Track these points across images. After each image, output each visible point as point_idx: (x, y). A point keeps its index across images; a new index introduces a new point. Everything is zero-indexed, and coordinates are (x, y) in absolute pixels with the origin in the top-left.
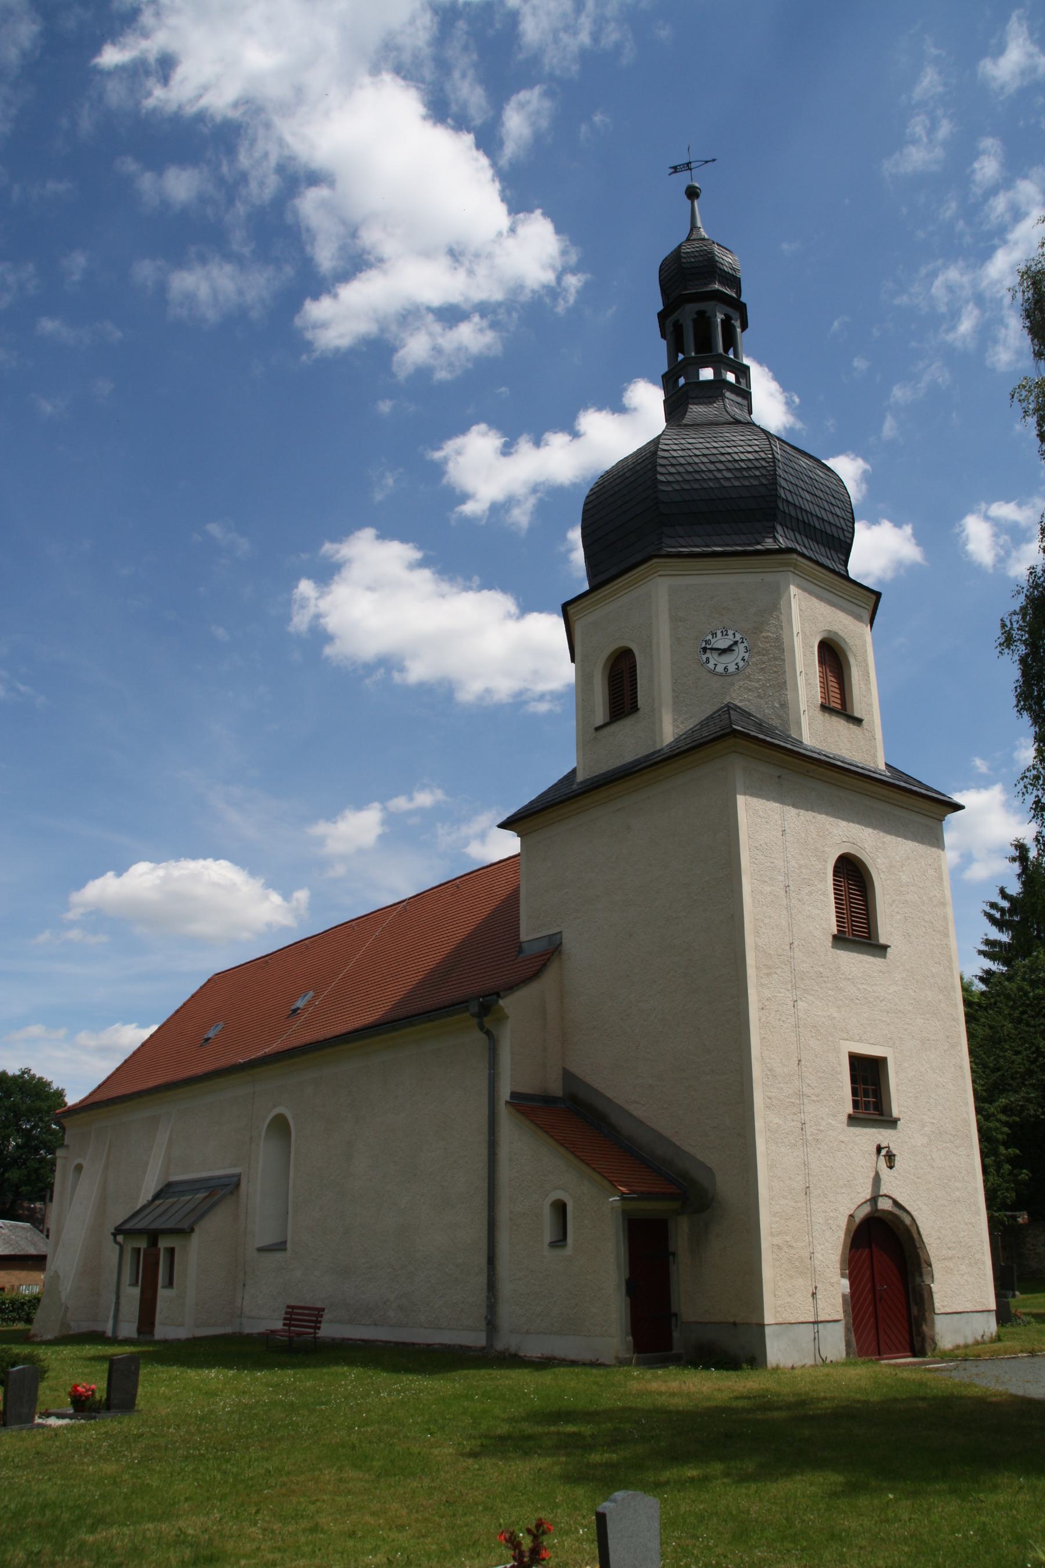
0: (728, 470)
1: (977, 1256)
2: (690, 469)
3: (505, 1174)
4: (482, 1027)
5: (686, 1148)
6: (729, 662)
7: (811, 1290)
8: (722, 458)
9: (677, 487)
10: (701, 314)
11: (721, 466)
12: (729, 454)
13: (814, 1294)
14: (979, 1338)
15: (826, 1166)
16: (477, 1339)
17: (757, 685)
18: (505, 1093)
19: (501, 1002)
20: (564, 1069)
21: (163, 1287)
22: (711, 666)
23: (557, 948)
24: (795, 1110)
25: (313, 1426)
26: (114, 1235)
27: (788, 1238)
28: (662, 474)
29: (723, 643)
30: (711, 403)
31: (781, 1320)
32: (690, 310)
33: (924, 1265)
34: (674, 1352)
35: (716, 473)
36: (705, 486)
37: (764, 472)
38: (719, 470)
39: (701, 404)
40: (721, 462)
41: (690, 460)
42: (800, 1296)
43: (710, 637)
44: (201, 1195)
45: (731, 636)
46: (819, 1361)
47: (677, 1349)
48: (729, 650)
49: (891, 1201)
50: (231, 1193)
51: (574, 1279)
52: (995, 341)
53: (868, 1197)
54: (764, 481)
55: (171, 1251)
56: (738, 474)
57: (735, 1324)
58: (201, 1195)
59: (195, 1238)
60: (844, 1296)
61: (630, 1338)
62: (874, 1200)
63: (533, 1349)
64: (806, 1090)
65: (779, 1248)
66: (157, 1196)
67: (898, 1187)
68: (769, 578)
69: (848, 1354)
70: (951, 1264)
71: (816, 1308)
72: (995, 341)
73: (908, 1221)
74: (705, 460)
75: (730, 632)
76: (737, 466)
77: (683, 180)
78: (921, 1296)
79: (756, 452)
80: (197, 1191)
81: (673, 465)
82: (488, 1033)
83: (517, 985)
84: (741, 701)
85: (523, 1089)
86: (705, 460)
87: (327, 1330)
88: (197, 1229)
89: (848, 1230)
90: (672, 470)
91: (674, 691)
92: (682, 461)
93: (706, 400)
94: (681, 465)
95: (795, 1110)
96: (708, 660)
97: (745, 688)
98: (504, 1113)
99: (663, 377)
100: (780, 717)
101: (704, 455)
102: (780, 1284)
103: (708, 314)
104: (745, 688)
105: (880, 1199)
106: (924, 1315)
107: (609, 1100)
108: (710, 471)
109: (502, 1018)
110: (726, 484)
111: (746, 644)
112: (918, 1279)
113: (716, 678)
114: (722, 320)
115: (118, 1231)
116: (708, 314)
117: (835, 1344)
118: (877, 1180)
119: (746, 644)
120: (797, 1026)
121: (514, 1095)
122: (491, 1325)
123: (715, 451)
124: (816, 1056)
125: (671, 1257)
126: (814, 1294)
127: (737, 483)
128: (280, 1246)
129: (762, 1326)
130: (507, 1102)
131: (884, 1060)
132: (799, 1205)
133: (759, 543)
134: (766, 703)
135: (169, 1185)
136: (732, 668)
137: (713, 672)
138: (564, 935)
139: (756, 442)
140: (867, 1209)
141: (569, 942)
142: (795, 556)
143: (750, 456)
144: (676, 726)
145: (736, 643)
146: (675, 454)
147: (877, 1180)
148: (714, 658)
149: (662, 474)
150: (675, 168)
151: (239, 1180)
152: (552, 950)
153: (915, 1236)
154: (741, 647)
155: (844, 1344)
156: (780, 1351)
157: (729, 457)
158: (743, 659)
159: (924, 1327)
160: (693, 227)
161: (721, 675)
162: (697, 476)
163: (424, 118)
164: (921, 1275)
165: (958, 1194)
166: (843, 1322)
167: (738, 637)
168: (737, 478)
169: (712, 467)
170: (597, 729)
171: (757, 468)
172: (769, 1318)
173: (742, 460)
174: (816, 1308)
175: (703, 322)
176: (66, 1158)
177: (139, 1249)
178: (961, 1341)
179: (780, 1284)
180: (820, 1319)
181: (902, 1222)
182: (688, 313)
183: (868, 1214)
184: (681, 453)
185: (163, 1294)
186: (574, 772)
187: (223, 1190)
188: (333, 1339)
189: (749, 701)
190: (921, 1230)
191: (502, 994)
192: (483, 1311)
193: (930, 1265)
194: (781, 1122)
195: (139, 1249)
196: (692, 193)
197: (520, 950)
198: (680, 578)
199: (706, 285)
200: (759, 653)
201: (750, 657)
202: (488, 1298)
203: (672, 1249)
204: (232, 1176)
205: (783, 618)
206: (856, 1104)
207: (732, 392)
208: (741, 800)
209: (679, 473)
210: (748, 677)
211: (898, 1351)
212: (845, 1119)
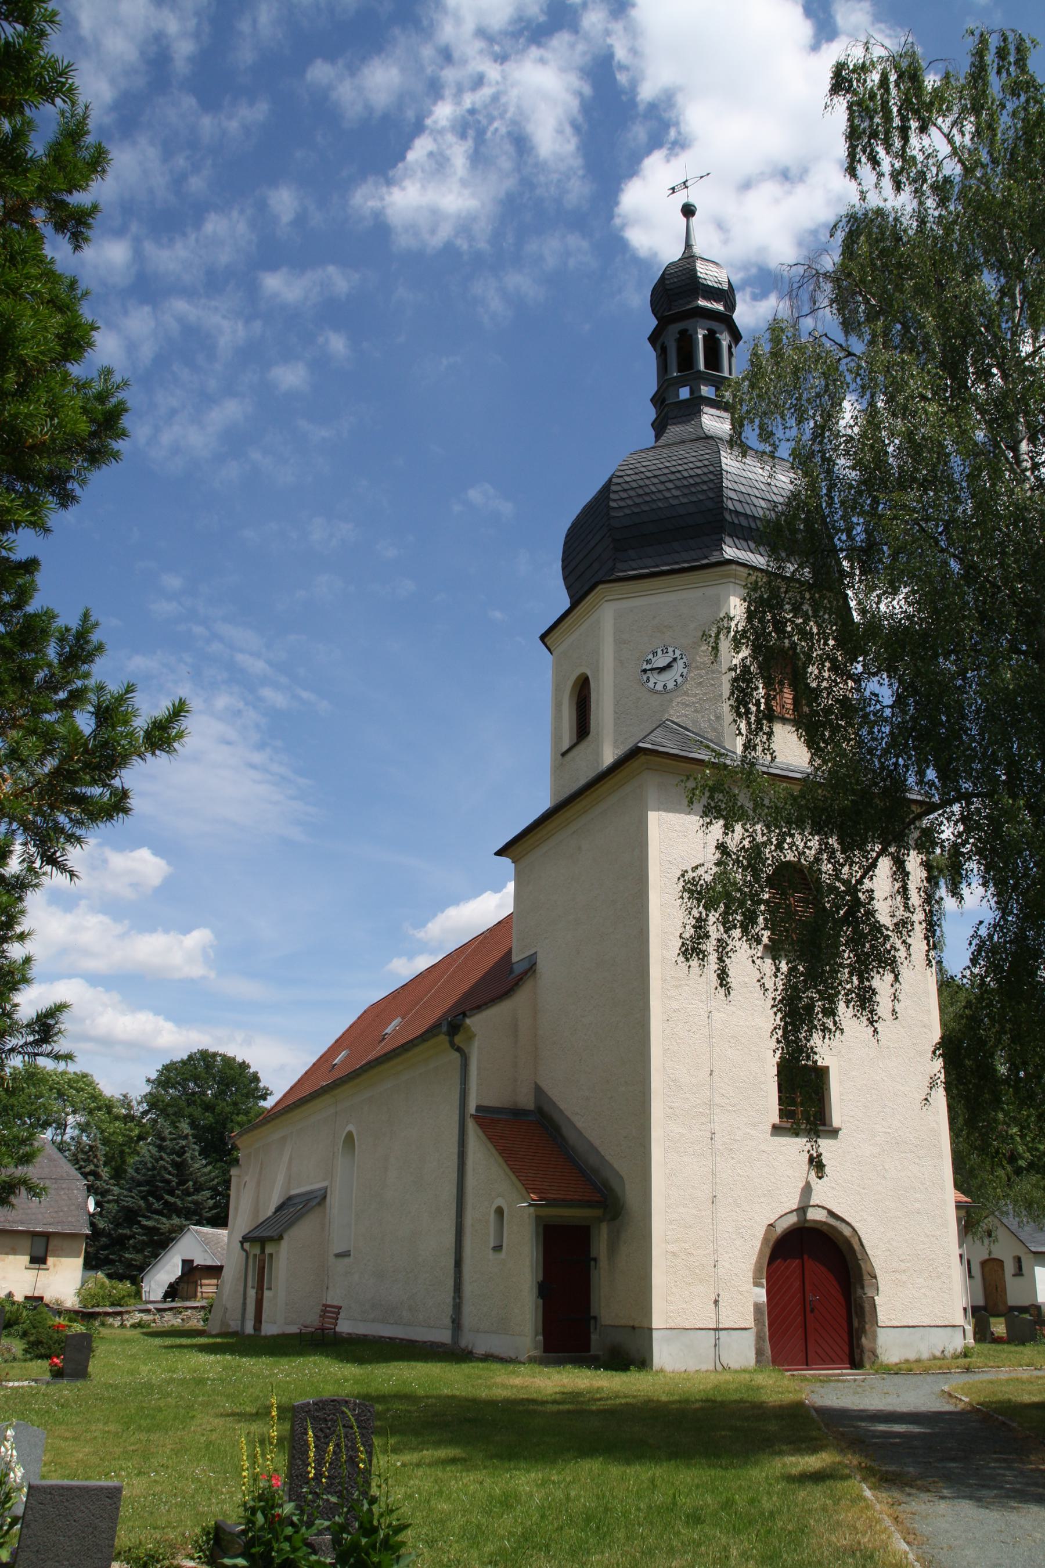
0: (677, 488)
1: (941, 1269)
2: (640, 492)
3: (471, 1181)
5: (608, 1158)
6: (668, 679)
7: (713, 1297)
8: (672, 477)
9: (628, 511)
11: (670, 485)
12: (679, 471)
13: (716, 1302)
14: (938, 1354)
15: (740, 1176)
16: (444, 1336)
17: (694, 700)
18: (472, 1109)
19: (468, 1021)
20: (536, 1084)
22: (651, 685)
23: (531, 968)
24: (703, 1119)
26: (242, 1243)
27: (686, 1246)
28: (615, 500)
29: (661, 661)
30: (689, 421)
31: (672, 1325)
33: (866, 1277)
34: (592, 1353)
35: (665, 493)
36: (654, 506)
37: (712, 485)
38: (668, 489)
39: (679, 423)
40: (671, 481)
41: (641, 483)
42: (700, 1301)
43: (651, 656)
45: (671, 654)
46: (719, 1368)
47: (595, 1350)
48: (669, 666)
49: (825, 1212)
50: (319, 1204)
51: (509, 1282)
52: (771, 340)
53: (795, 1207)
54: (711, 495)
55: (271, 1255)
56: (686, 491)
57: (633, 1328)
59: (284, 1244)
60: (757, 1307)
61: (540, 1338)
62: (802, 1210)
63: (480, 1350)
64: (717, 1100)
65: (674, 1254)
66: (279, 1208)
67: (837, 1198)
68: (710, 591)
69: (758, 1361)
70: (904, 1278)
71: (717, 1314)
72: (771, 340)
73: (847, 1232)
74: (655, 481)
75: (670, 650)
76: (686, 483)
77: (681, 198)
78: (862, 1308)
79: (705, 466)
81: (625, 490)
82: (459, 1050)
83: (486, 1004)
84: (678, 717)
85: (486, 1103)
86: (655, 481)
87: (344, 1327)
88: (285, 1237)
89: (765, 1240)
91: (616, 713)
92: (634, 485)
93: (684, 419)
94: (633, 489)
95: (703, 1119)
96: (648, 679)
97: (683, 704)
98: (471, 1126)
99: (652, 400)
100: (715, 730)
101: (655, 476)
102: (674, 1290)
103: (690, 332)
104: (683, 704)
105: (810, 1210)
106: (864, 1327)
107: (561, 1111)
108: (660, 491)
109: (471, 1037)
111: (685, 660)
112: (859, 1291)
113: (655, 696)
114: (704, 336)
116: (690, 332)
117: (742, 1352)
118: (807, 1190)
119: (685, 660)
120: (710, 1037)
121: (479, 1108)
122: (456, 1323)
123: (666, 471)
124: (734, 1066)
125: (592, 1263)
126: (716, 1302)
127: (684, 500)
129: (651, 1329)
130: (472, 1115)
132: (703, 1213)
133: (706, 558)
134: (703, 717)
135: (290, 1198)
136: (671, 685)
137: (653, 691)
138: (538, 954)
139: (707, 456)
140: (793, 1219)
141: (542, 965)
142: (734, 567)
143: (699, 471)
144: (616, 747)
145: (675, 659)
146: (628, 479)
147: (807, 1190)
148: (654, 678)
149: (615, 500)
150: (673, 189)
151: (326, 1192)
152: (531, 968)
153: (857, 1247)
154: (680, 663)
155: (754, 1352)
156: (666, 1356)
157: (678, 475)
158: (682, 676)
159: (864, 1340)
161: (660, 693)
162: (647, 499)
164: (863, 1288)
165: (917, 1205)
166: (754, 1330)
167: (678, 653)
169: (662, 487)
170: (564, 754)
171: (705, 482)
172: (657, 1322)
173: (691, 476)
174: (717, 1314)
175: (686, 341)
176: (239, 1176)
178: (912, 1356)
179: (674, 1290)
180: (721, 1326)
181: (841, 1233)
182: (673, 331)
183: (794, 1224)
184: (634, 477)
187: (317, 1200)
188: (374, 1337)
189: (686, 716)
190: (864, 1241)
191: (468, 1013)
192: (449, 1311)
193: (875, 1277)
194: (684, 1132)
196: (688, 211)
197: (511, 971)
198: (624, 601)
199: (689, 303)
200: (697, 668)
201: (689, 672)
202: (454, 1298)
203: (593, 1254)
204: (320, 1190)
206: (782, 1114)
207: (712, 407)
208: (653, 817)
209: (630, 497)
210: (686, 693)
211: (833, 1362)
212: (769, 1129)
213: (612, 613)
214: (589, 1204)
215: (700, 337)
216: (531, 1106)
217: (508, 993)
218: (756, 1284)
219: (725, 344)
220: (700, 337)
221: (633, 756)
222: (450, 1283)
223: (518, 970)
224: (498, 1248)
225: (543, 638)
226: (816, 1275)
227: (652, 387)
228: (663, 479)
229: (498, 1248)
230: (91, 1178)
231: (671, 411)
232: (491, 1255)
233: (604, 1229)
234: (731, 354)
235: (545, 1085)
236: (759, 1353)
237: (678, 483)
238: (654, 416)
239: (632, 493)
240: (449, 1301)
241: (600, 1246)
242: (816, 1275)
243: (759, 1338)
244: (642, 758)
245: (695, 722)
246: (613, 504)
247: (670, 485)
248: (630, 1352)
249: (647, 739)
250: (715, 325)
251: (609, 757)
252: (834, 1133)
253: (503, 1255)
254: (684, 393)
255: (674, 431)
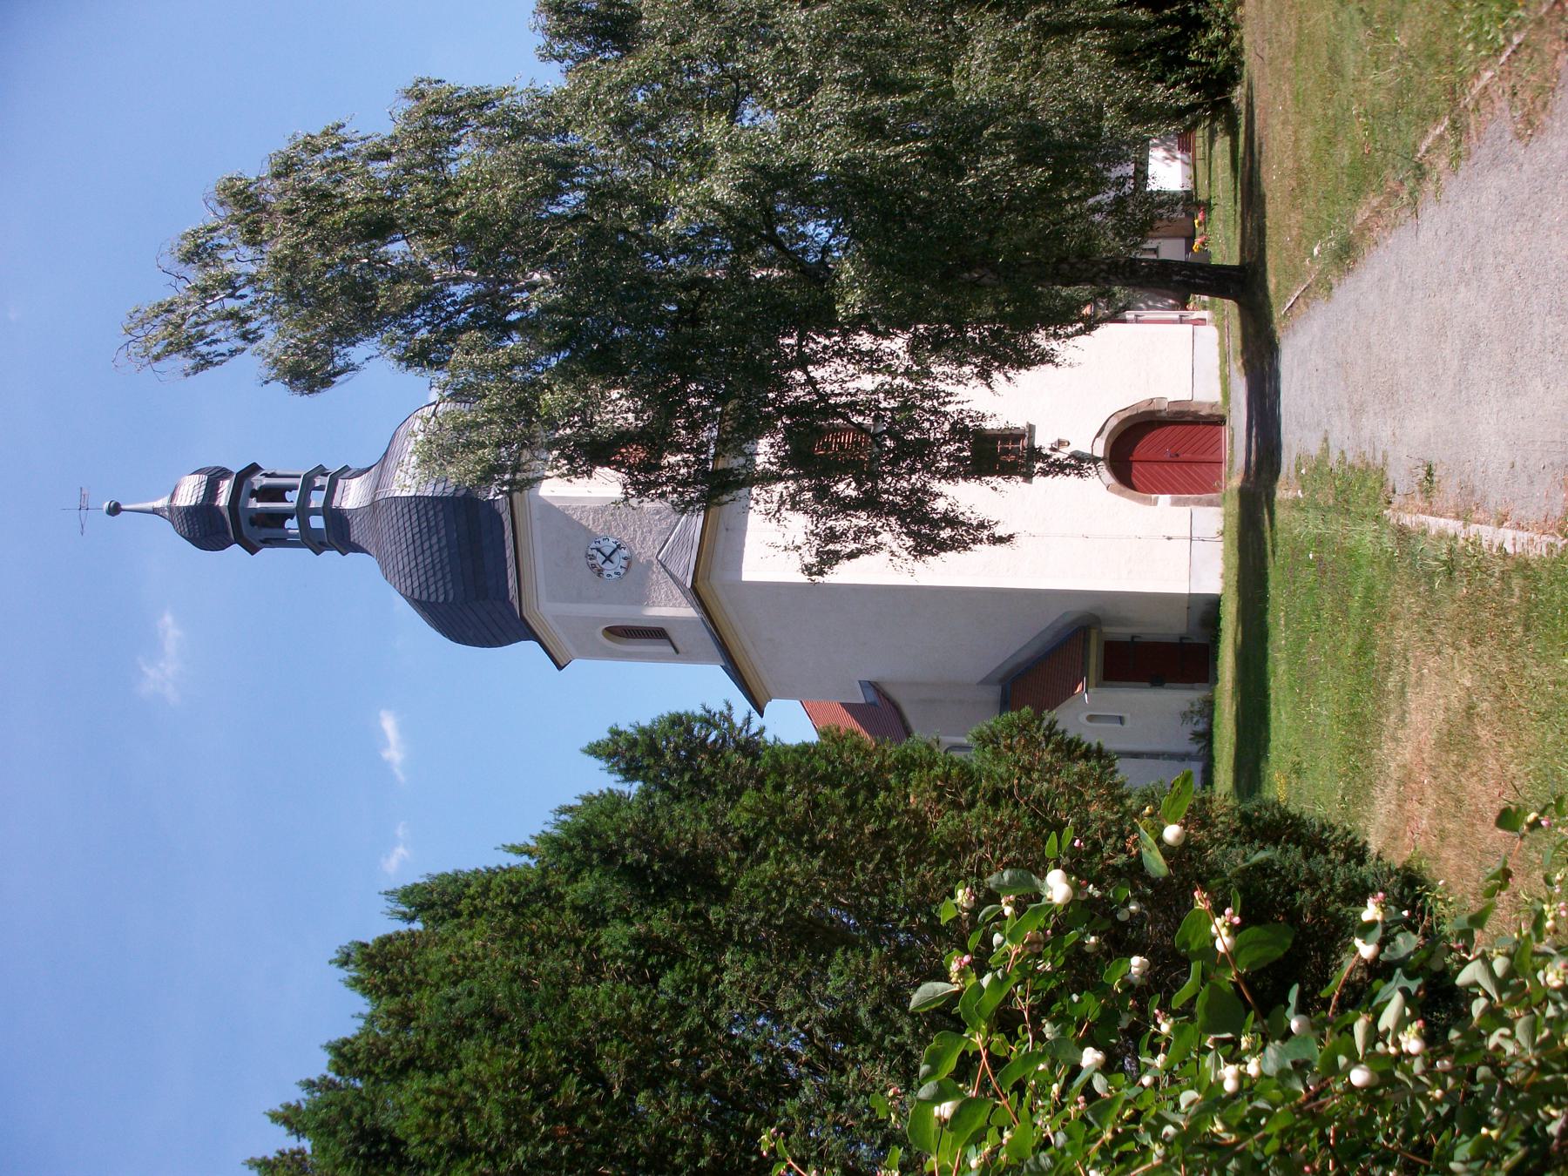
2: (431, 573)
8: (418, 543)
10: (253, 522)
11: (426, 545)
21: (1216, 421)
33: (1151, 408)
38: (431, 547)
42: (1165, 551)
60: (1175, 503)
73: (1114, 422)
78: (1177, 413)
86: (420, 559)
89: (1119, 493)
90: (432, 588)
92: (423, 578)
110: (444, 542)
122: (1183, 757)
127: (443, 532)
143: (415, 517)
146: (416, 584)
152: (874, 686)
153: (1127, 414)
160: (155, 511)
168: (438, 532)
169: (428, 553)
196: (115, 510)
197: (874, 704)
205: (575, 505)
210: (633, 540)
213: (543, 601)
214: (1086, 640)
215: (259, 505)
216: (998, 689)
217: (896, 708)
218: (1156, 503)
219: (266, 481)
220: (259, 505)
221: (697, 595)
222: (1151, 762)
223: (872, 697)
224: (1121, 720)
225: (560, 668)
226: (1146, 449)
227: (307, 553)
228: (419, 551)
229: (1121, 720)
230: (504, 360)
231: (338, 534)
232: (1127, 725)
233: (1106, 629)
234: (273, 475)
235: (980, 678)
236: (1210, 503)
237: (425, 537)
238: (336, 553)
239: (432, 580)
240: (1167, 763)
241: (1120, 632)
242: (1146, 449)
243: (1198, 503)
244: (703, 590)
245: (660, 533)
246: (441, 599)
247: (426, 545)
248: (1208, 609)
249: (682, 579)
250: (244, 491)
251: (689, 612)
252: (1031, 428)
253: (1127, 716)
254: (317, 522)
255: (356, 535)
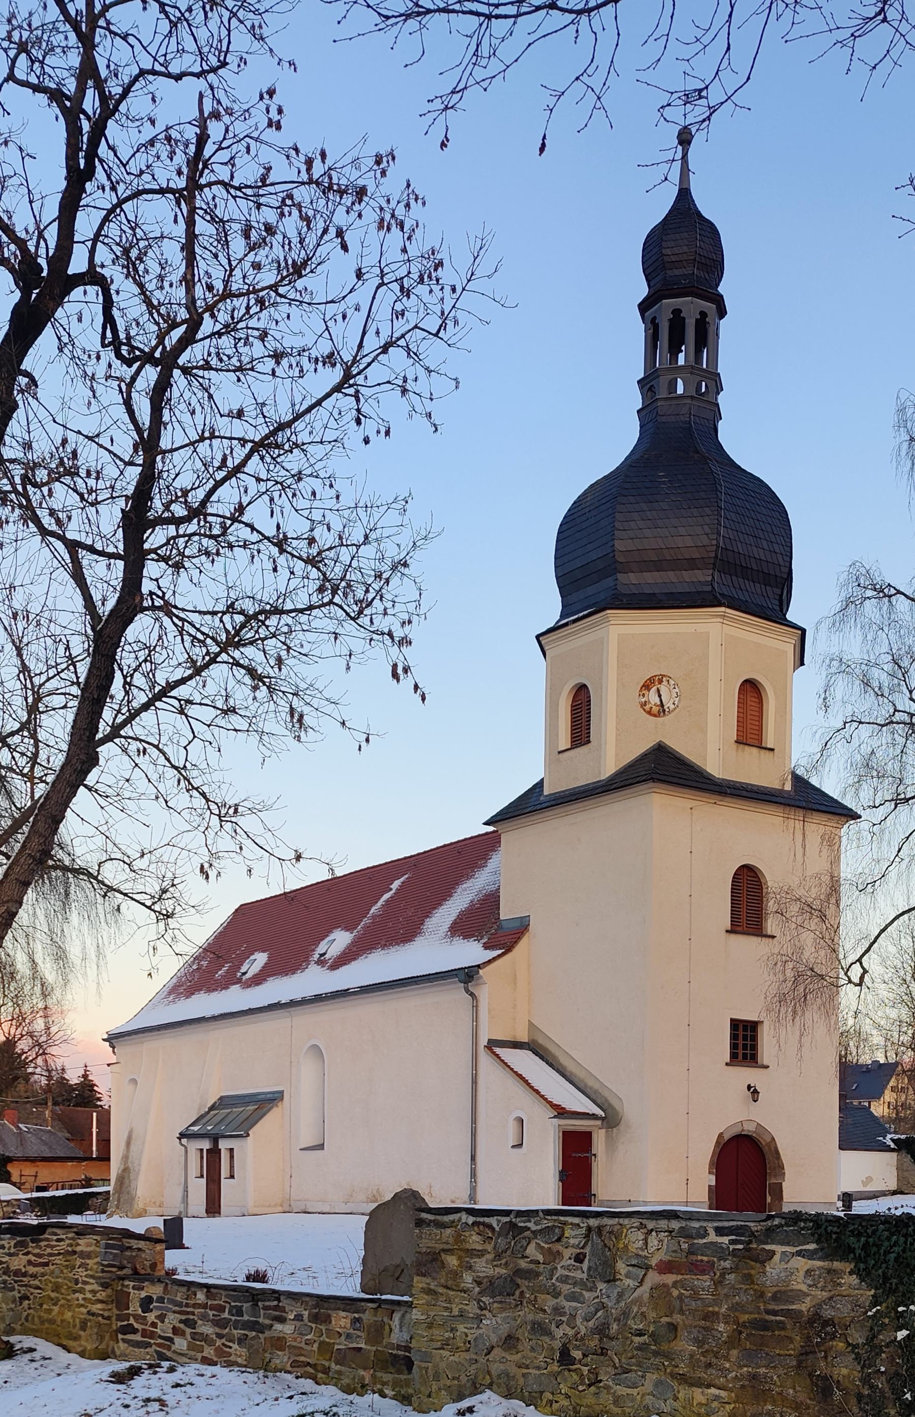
4: (467, 990)
10: (677, 312)
18: (483, 1042)
25: (254, 1326)
32: (670, 303)
44: (252, 1108)
58: (252, 1108)
80: (248, 1103)
82: (472, 995)
115: (182, 1136)
128: (321, 1147)
131: (841, 1148)
163: (721, 1135)
170: (559, 752)
177: (202, 1150)
185: (226, 1184)
186: (540, 785)
187: (265, 1102)
195: (202, 1150)
